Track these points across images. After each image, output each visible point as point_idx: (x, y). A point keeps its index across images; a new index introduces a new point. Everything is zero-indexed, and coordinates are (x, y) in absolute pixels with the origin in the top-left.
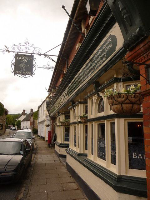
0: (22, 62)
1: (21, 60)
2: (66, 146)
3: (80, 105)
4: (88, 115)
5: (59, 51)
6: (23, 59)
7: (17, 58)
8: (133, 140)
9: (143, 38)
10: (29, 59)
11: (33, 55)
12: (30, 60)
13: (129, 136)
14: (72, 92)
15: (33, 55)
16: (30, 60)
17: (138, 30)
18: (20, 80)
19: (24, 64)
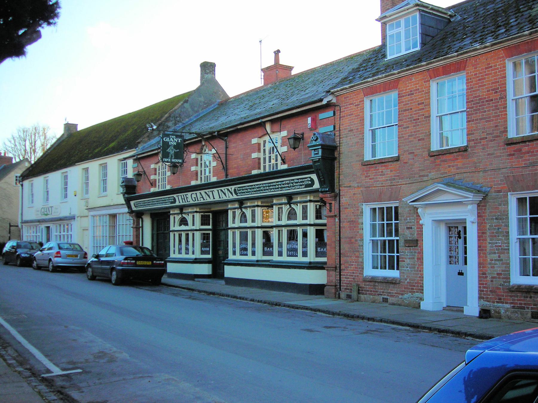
0: (171, 145)
1: (169, 142)
2: (207, 261)
3: (433, 85)
4: (236, 249)
5: (131, 112)
6: (171, 141)
7: (164, 140)
8: (319, 240)
9: (19, 261)
10: (178, 140)
11: (183, 134)
12: (179, 141)
13: (316, 238)
14: (255, 193)
15: (183, 134)
16: (179, 141)
17: (15, 318)
18: (75, 196)
19: (173, 148)
